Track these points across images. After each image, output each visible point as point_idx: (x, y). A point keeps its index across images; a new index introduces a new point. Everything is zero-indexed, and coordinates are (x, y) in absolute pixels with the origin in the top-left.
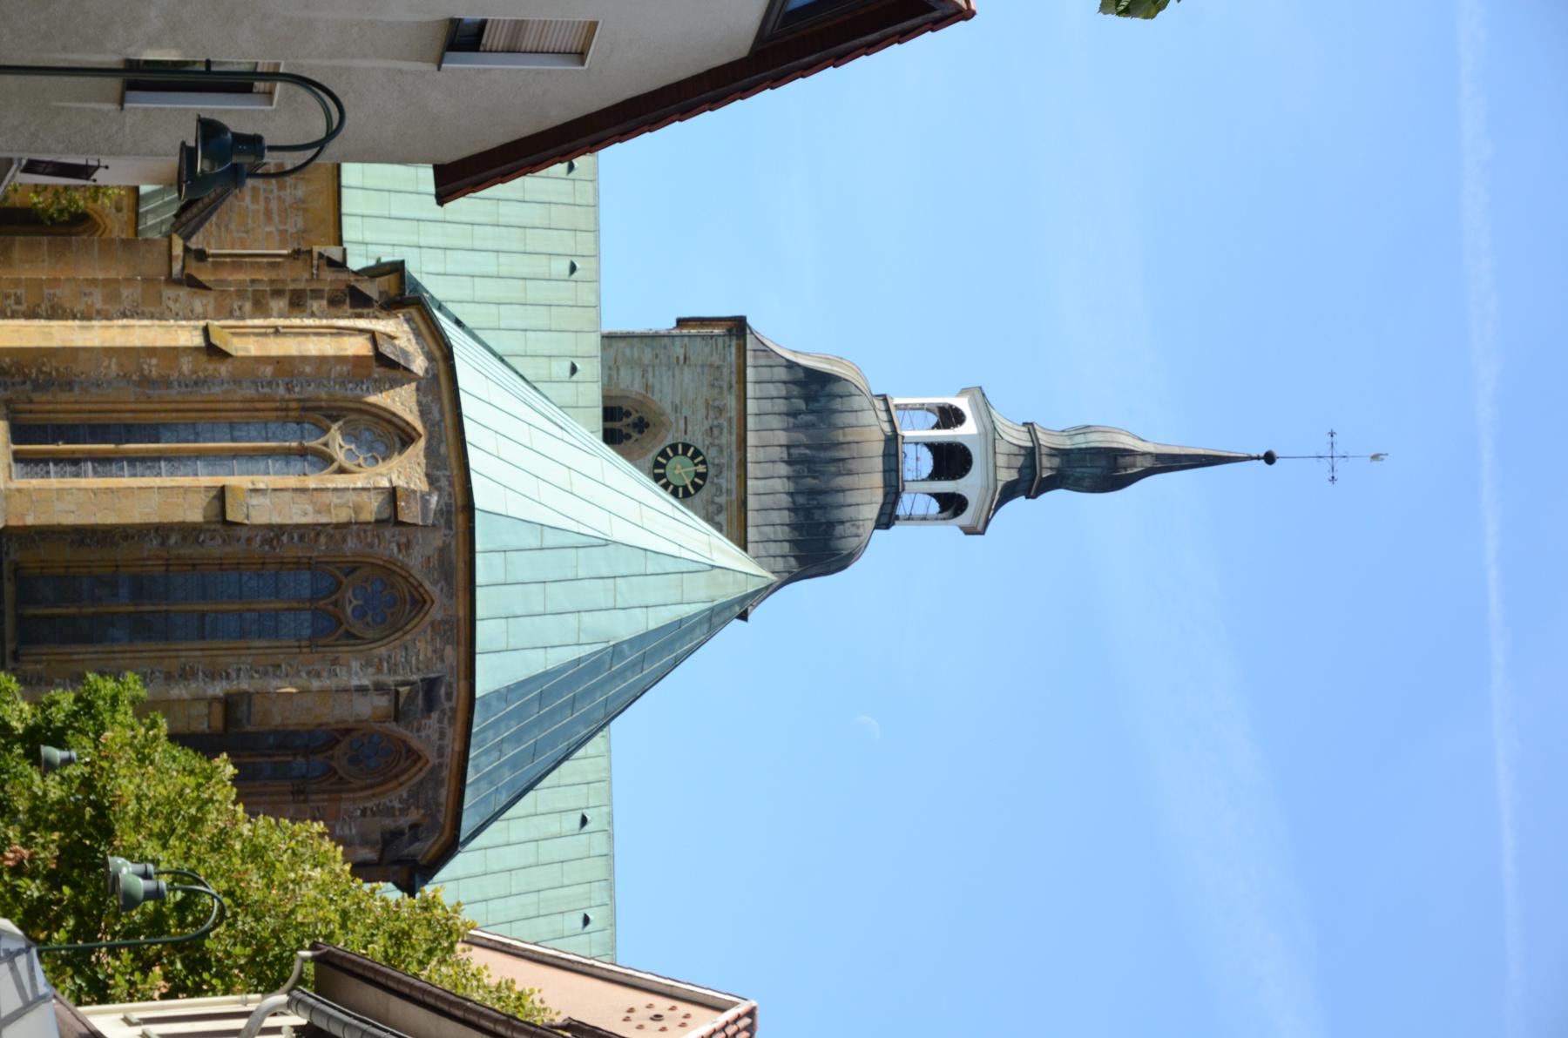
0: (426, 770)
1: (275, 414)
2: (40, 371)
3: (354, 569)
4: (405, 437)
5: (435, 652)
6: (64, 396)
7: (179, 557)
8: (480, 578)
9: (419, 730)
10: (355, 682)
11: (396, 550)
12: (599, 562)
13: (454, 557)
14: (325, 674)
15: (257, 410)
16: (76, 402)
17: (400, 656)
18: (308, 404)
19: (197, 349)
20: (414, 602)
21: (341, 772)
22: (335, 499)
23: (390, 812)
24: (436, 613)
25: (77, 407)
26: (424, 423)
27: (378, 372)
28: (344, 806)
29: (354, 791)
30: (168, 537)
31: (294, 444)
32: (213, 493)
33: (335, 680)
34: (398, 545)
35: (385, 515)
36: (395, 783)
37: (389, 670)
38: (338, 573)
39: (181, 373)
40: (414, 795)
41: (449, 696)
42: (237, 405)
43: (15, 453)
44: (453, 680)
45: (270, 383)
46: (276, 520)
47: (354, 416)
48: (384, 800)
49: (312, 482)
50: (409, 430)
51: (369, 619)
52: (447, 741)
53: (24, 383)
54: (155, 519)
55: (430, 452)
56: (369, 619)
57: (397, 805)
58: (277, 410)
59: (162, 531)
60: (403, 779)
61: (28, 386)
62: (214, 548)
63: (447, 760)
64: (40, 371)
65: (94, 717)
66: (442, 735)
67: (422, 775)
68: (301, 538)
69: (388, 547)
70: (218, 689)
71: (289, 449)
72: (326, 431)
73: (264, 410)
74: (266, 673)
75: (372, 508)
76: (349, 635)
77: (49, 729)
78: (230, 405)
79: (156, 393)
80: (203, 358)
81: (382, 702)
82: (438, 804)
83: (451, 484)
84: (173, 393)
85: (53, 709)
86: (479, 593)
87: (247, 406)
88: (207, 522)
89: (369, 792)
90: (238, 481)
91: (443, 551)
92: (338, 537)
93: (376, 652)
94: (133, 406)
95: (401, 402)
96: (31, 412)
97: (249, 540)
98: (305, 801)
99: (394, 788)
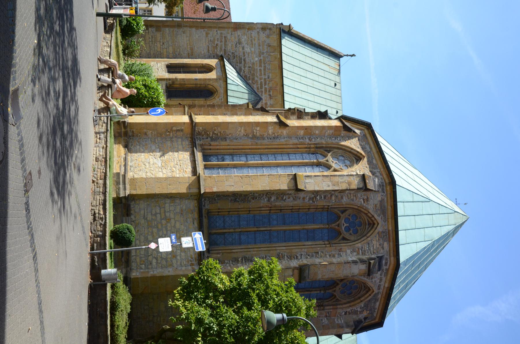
0: (372, 295)
1: (305, 150)
2: (214, 133)
3: (346, 210)
4: (358, 158)
5: (380, 245)
6: (223, 143)
7: (275, 206)
8: (400, 213)
9: (372, 279)
10: (350, 259)
11: (362, 201)
12: (427, 208)
13: (386, 204)
14: (336, 256)
15: (298, 148)
16: (228, 145)
17: (366, 247)
18: (318, 146)
19: (275, 123)
20: (369, 224)
21: (338, 297)
22: (340, 180)
23: (356, 312)
24: (380, 229)
25: (229, 147)
26: (365, 152)
27: (343, 133)
28: (339, 311)
29: (342, 304)
30: (271, 198)
31: (315, 161)
32: (291, 177)
33: (341, 258)
34: (363, 200)
35: (361, 186)
36: (359, 301)
37: (362, 253)
38: (339, 212)
39: (268, 134)
40: (366, 306)
41: (386, 264)
42: (291, 146)
43: (205, 165)
44: (388, 257)
45: (302, 138)
46: (317, 189)
47: (336, 150)
48: (354, 308)
49: (326, 173)
50: (359, 155)
51: (351, 232)
52: (382, 283)
53: (207, 138)
54: (268, 188)
55: (370, 162)
56: (351, 232)
57: (359, 310)
58: (306, 148)
59: (268, 194)
60: (362, 299)
61: (209, 139)
62: (289, 202)
63: (381, 290)
64: (214, 133)
65: (263, 282)
66: (381, 280)
67: (371, 297)
68: (325, 197)
69: (359, 201)
70: (295, 263)
71: (313, 162)
72: (325, 156)
73: (300, 148)
74: (313, 256)
75: (355, 183)
76: (344, 239)
77: (240, 289)
78: (288, 146)
79: (259, 142)
80: (277, 127)
81: (363, 267)
82: (375, 309)
83: (381, 174)
84: (266, 142)
85: (241, 278)
86: (400, 219)
87: (294, 146)
88: (289, 190)
89: (348, 305)
90: (302, 172)
91: (382, 201)
92: (339, 197)
93: (357, 245)
94: (250, 147)
95: (353, 144)
96: (210, 149)
97: (304, 198)
98: (323, 310)
99: (358, 303)
